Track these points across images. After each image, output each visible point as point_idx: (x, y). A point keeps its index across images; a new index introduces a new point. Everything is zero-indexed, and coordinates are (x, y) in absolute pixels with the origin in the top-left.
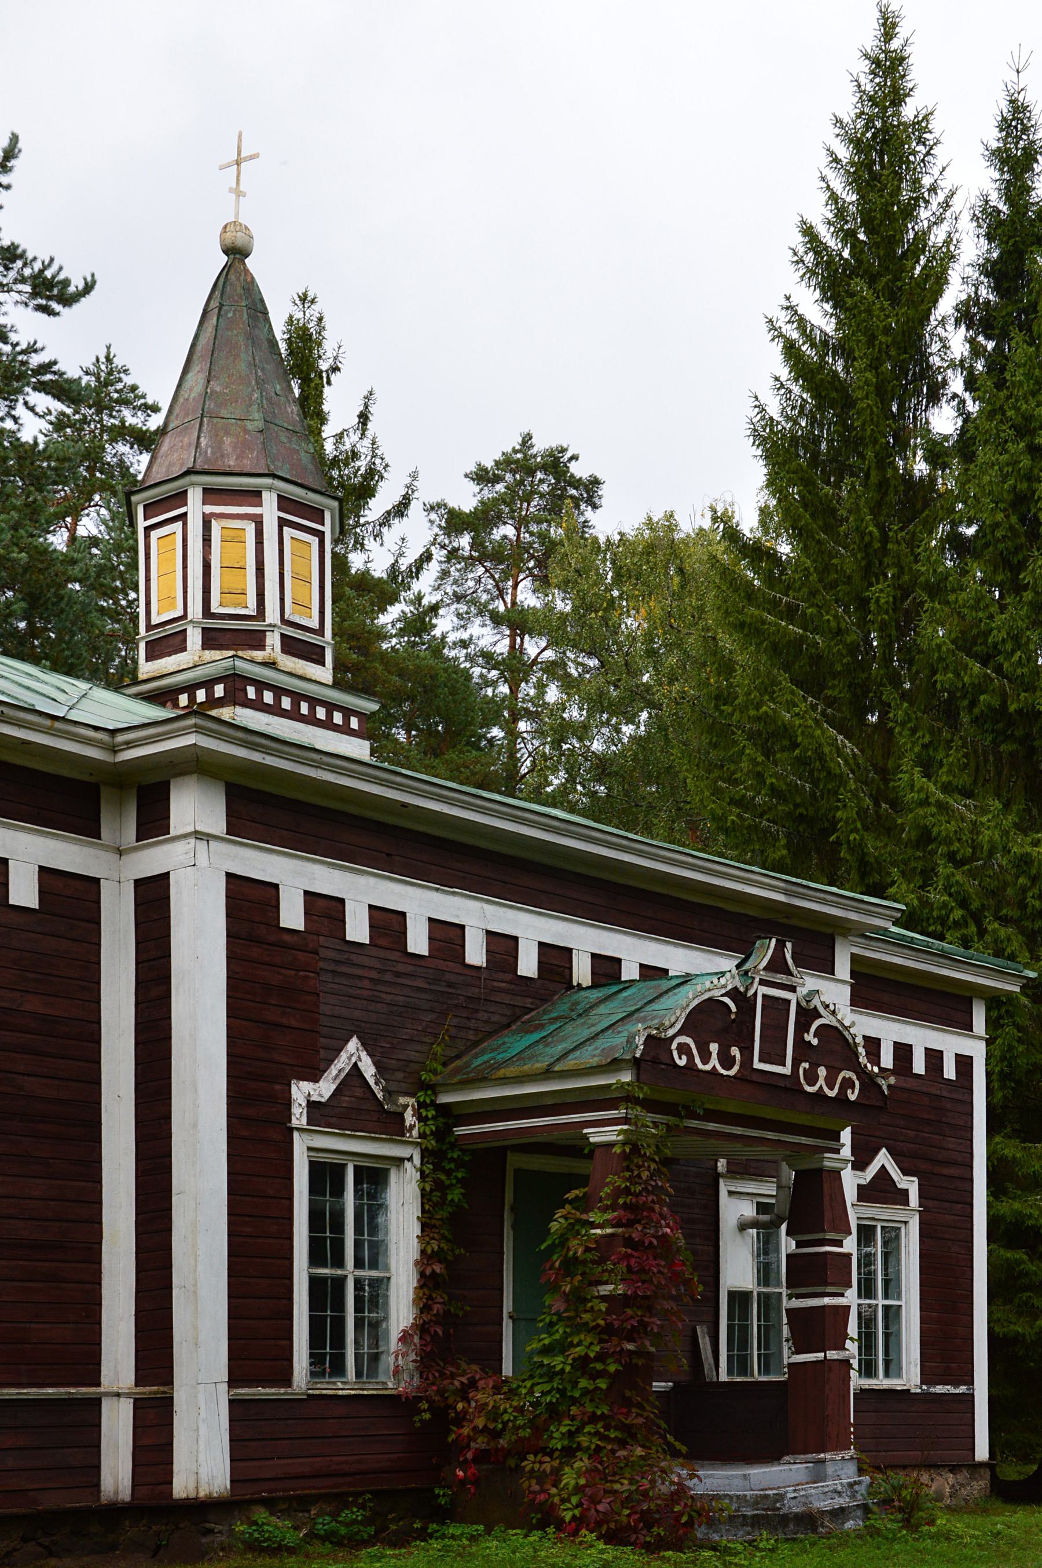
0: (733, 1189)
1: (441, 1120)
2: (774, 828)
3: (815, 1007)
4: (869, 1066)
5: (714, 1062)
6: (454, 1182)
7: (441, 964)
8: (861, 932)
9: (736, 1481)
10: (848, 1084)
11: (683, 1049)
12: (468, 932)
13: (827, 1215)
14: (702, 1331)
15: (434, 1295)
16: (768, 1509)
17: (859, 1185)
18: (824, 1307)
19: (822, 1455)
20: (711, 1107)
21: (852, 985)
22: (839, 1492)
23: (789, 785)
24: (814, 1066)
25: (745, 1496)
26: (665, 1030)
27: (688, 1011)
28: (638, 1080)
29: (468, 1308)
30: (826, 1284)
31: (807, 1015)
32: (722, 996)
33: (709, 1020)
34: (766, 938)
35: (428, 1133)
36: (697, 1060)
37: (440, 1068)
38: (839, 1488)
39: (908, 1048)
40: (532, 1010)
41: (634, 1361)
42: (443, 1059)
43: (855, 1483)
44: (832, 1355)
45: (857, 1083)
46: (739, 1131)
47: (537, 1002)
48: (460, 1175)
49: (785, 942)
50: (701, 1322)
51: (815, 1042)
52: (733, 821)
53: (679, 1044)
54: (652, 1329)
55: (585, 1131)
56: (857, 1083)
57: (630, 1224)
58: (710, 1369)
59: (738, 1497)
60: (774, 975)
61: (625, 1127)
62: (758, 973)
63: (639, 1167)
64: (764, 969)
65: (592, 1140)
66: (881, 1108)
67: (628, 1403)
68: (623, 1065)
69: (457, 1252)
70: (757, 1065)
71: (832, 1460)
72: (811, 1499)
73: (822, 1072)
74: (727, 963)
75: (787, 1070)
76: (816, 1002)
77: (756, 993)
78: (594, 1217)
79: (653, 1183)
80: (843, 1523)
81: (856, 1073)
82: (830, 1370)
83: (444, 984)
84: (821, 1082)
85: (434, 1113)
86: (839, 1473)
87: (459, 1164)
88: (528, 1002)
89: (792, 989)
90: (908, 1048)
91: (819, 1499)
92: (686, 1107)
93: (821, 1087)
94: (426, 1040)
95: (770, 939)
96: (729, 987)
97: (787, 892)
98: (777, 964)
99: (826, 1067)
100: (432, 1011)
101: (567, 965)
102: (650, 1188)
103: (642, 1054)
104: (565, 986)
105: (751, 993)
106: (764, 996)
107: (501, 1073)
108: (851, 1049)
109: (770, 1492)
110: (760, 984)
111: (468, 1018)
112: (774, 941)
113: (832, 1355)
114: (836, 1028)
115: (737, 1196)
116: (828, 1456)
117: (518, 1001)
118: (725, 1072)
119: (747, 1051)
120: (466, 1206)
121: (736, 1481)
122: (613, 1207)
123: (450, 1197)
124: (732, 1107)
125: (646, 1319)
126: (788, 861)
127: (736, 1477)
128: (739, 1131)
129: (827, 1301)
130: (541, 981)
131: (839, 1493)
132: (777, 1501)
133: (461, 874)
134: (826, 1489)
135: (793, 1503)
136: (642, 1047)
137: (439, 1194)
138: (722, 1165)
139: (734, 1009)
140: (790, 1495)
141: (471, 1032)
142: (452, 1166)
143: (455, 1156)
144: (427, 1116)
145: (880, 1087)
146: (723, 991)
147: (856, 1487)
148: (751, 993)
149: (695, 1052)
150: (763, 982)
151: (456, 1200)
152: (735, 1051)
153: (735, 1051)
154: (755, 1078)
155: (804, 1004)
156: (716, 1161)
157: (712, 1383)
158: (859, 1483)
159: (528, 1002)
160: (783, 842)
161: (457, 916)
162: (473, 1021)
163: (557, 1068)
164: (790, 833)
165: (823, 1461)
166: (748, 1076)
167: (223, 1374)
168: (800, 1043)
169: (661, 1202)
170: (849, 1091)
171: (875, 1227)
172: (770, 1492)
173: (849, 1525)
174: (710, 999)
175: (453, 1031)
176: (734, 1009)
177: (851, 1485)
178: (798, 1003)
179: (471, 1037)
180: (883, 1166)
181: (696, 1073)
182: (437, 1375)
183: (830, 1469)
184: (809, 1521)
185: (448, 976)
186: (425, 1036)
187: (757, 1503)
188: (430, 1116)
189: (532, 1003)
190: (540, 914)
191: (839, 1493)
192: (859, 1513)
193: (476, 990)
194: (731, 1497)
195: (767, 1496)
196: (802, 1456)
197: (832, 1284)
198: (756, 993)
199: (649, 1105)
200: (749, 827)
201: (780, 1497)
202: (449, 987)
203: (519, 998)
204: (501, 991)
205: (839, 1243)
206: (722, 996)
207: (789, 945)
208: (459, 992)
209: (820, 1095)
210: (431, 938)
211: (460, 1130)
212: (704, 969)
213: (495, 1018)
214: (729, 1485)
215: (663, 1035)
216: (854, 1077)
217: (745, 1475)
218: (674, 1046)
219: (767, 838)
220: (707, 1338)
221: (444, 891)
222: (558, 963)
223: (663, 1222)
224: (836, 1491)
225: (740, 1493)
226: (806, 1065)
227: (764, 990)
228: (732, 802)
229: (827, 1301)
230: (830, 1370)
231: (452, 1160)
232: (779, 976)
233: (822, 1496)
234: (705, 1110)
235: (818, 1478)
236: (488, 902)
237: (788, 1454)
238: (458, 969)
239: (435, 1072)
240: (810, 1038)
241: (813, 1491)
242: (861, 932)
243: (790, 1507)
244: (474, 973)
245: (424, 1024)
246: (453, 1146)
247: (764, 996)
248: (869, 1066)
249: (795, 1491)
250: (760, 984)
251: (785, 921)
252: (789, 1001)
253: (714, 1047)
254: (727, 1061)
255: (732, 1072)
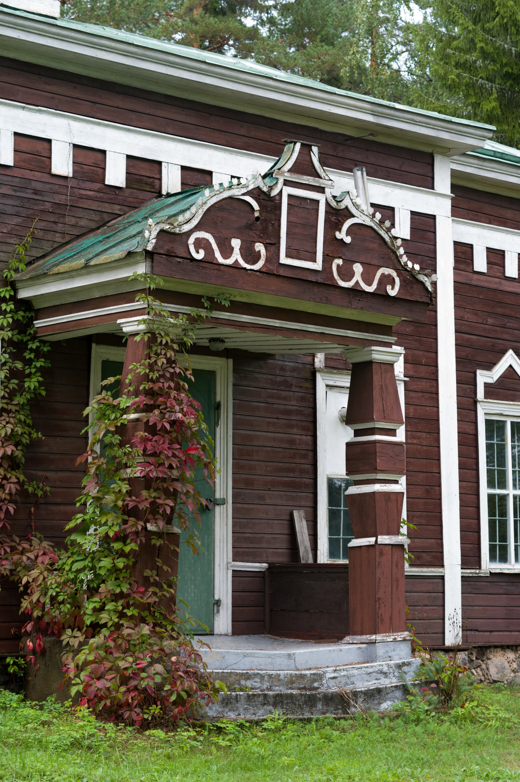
0: (331, 383)
1: (21, 313)
2: (488, 85)
3: (347, 208)
4: (410, 264)
5: (236, 256)
6: (33, 370)
7: (28, 174)
8: (463, 152)
9: (279, 661)
10: (387, 280)
11: (200, 244)
12: (55, 146)
13: (377, 405)
14: (300, 515)
15: (9, 476)
16: (304, 688)
17: (485, 383)
18: (373, 494)
19: (374, 637)
20: (238, 299)
21: (453, 199)
22: (385, 673)
23: (496, 49)
24: (349, 262)
25: (279, 675)
26: (180, 226)
27: (206, 208)
28: (152, 272)
29: (48, 489)
30: (375, 470)
31: (337, 215)
32: (243, 195)
33: (226, 216)
34: (291, 142)
35: (5, 325)
36: (218, 255)
37: (22, 266)
38: (385, 669)
39: (501, 254)
40: (120, 215)
41: (153, 542)
42: (27, 259)
43: (404, 664)
44: (384, 539)
45: (397, 280)
46: (277, 323)
47: (126, 209)
48: (38, 365)
49: (310, 146)
50: (299, 507)
51: (348, 240)
52: (453, 80)
53: (197, 239)
54: (165, 510)
55: (119, 321)
56: (397, 280)
57: (148, 409)
58: (306, 551)
59: (270, 676)
60: (300, 176)
61: (146, 317)
62: (282, 174)
63: (156, 354)
64: (289, 171)
65: (125, 330)
66: (428, 304)
67: (147, 582)
68: (138, 258)
69: (35, 435)
70: (284, 260)
71: (383, 642)
72: (352, 679)
73: (358, 268)
74: (262, 165)
75: (318, 266)
76: (347, 202)
77: (280, 193)
78: (124, 402)
79: (172, 370)
80: (380, 704)
81: (396, 270)
82: (381, 554)
83: (31, 191)
84: (357, 277)
85: (13, 307)
86: (390, 654)
87: (38, 353)
88: (116, 209)
89: (321, 190)
90: (501, 254)
91: (362, 680)
92: (210, 299)
93: (357, 282)
94: (12, 241)
95: (295, 143)
96: (251, 187)
97: (374, 114)
98: (303, 167)
99: (362, 263)
100: (17, 215)
101: (157, 176)
102: (168, 375)
103: (154, 248)
104: (156, 195)
105: (275, 193)
106: (290, 196)
107: (56, 270)
108: (388, 247)
109: (307, 672)
110: (285, 184)
111: (55, 223)
112: (298, 146)
113: (384, 539)
114: (371, 228)
115: (336, 389)
116: (379, 637)
117: (107, 208)
118: (248, 267)
119: (273, 245)
120: (44, 393)
121: (279, 661)
122: (136, 393)
123: (26, 385)
124: (267, 300)
125: (159, 501)
126: (499, 112)
127: (279, 656)
128: (277, 323)
129: (377, 487)
130: (129, 191)
131: (385, 674)
132: (315, 681)
133: (51, 95)
134: (371, 670)
135: (332, 683)
136: (154, 241)
137: (16, 381)
138: (319, 360)
139: (256, 206)
140: (328, 675)
141: (58, 235)
142: (32, 356)
143: (34, 347)
144: (5, 310)
145: (422, 284)
146: (244, 191)
147: (405, 669)
148: (275, 193)
149: (215, 246)
150: (287, 183)
151: (32, 387)
152: (260, 247)
153: (260, 247)
154: (282, 272)
155: (333, 204)
156: (313, 356)
157: (307, 566)
158: (409, 664)
159: (116, 209)
160: (495, 95)
161: (44, 131)
162: (60, 225)
163: (92, 263)
164: (502, 89)
165: (373, 643)
166: (274, 272)
167: (460, 563)
168: (331, 241)
169: (178, 388)
170: (389, 288)
171: (504, 422)
172: (307, 672)
173: (385, 706)
174: (230, 198)
175: (39, 234)
176: (256, 206)
177: (399, 666)
178: (327, 204)
179: (57, 240)
180: (511, 366)
181: (216, 267)
182: (8, 550)
183: (380, 650)
184: (340, 702)
185: (34, 185)
186: (11, 238)
187: (292, 682)
188: (8, 310)
189: (120, 210)
190: (129, 130)
191: (385, 674)
192: (398, 694)
193: (64, 197)
194: (262, 677)
195: (302, 676)
196: (359, 637)
197: (383, 471)
198: (281, 191)
199: (160, 294)
200: (467, 85)
201: (319, 677)
202: (36, 194)
203: (106, 205)
204: (89, 198)
205: (392, 432)
206: (243, 195)
207: (315, 149)
208: (45, 199)
209: (356, 291)
210: (16, 151)
211: (39, 323)
212: (236, 169)
213: (83, 223)
214: (271, 664)
215: (177, 230)
216: (394, 274)
217: (289, 655)
218: (191, 241)
219: (482, 93)
220: (304, 523)
221: (30, 109)
222: (148, 174)
223: (177, 408)
224: (381, 672)
225: (273, 672)
226: (340, 262)
227: (288, 190)
228: (458, 65)
229: (377, 487)
230: (381, 554)
231: (31, 350)
232: (305, 177)
233: (366, 677)
234: (231, 302)
235: (370, 659)
236: (75, 119)
237: (349, 634)
238: (46, 178)
239: (17, 270)
240: (342, 235)
241: (355, 672)
242: (463, 152)
243: (329, 687)
244: (62, 182)
245: (9, 227)
246: (34, 338)
247: (290, 196)
248: (410, 264)
249: (335, 671)
250: (285, 184)
251: (371, 138)
252: (318, 202)
253: (236, 243)
254: (251, 256)
255: (257, 267)
